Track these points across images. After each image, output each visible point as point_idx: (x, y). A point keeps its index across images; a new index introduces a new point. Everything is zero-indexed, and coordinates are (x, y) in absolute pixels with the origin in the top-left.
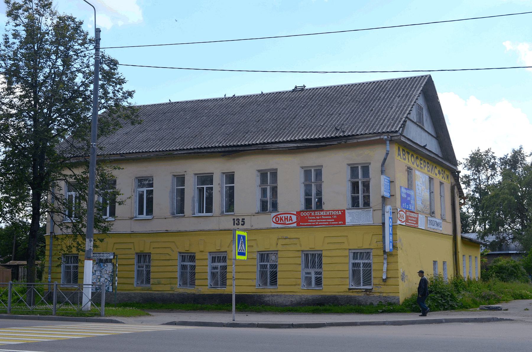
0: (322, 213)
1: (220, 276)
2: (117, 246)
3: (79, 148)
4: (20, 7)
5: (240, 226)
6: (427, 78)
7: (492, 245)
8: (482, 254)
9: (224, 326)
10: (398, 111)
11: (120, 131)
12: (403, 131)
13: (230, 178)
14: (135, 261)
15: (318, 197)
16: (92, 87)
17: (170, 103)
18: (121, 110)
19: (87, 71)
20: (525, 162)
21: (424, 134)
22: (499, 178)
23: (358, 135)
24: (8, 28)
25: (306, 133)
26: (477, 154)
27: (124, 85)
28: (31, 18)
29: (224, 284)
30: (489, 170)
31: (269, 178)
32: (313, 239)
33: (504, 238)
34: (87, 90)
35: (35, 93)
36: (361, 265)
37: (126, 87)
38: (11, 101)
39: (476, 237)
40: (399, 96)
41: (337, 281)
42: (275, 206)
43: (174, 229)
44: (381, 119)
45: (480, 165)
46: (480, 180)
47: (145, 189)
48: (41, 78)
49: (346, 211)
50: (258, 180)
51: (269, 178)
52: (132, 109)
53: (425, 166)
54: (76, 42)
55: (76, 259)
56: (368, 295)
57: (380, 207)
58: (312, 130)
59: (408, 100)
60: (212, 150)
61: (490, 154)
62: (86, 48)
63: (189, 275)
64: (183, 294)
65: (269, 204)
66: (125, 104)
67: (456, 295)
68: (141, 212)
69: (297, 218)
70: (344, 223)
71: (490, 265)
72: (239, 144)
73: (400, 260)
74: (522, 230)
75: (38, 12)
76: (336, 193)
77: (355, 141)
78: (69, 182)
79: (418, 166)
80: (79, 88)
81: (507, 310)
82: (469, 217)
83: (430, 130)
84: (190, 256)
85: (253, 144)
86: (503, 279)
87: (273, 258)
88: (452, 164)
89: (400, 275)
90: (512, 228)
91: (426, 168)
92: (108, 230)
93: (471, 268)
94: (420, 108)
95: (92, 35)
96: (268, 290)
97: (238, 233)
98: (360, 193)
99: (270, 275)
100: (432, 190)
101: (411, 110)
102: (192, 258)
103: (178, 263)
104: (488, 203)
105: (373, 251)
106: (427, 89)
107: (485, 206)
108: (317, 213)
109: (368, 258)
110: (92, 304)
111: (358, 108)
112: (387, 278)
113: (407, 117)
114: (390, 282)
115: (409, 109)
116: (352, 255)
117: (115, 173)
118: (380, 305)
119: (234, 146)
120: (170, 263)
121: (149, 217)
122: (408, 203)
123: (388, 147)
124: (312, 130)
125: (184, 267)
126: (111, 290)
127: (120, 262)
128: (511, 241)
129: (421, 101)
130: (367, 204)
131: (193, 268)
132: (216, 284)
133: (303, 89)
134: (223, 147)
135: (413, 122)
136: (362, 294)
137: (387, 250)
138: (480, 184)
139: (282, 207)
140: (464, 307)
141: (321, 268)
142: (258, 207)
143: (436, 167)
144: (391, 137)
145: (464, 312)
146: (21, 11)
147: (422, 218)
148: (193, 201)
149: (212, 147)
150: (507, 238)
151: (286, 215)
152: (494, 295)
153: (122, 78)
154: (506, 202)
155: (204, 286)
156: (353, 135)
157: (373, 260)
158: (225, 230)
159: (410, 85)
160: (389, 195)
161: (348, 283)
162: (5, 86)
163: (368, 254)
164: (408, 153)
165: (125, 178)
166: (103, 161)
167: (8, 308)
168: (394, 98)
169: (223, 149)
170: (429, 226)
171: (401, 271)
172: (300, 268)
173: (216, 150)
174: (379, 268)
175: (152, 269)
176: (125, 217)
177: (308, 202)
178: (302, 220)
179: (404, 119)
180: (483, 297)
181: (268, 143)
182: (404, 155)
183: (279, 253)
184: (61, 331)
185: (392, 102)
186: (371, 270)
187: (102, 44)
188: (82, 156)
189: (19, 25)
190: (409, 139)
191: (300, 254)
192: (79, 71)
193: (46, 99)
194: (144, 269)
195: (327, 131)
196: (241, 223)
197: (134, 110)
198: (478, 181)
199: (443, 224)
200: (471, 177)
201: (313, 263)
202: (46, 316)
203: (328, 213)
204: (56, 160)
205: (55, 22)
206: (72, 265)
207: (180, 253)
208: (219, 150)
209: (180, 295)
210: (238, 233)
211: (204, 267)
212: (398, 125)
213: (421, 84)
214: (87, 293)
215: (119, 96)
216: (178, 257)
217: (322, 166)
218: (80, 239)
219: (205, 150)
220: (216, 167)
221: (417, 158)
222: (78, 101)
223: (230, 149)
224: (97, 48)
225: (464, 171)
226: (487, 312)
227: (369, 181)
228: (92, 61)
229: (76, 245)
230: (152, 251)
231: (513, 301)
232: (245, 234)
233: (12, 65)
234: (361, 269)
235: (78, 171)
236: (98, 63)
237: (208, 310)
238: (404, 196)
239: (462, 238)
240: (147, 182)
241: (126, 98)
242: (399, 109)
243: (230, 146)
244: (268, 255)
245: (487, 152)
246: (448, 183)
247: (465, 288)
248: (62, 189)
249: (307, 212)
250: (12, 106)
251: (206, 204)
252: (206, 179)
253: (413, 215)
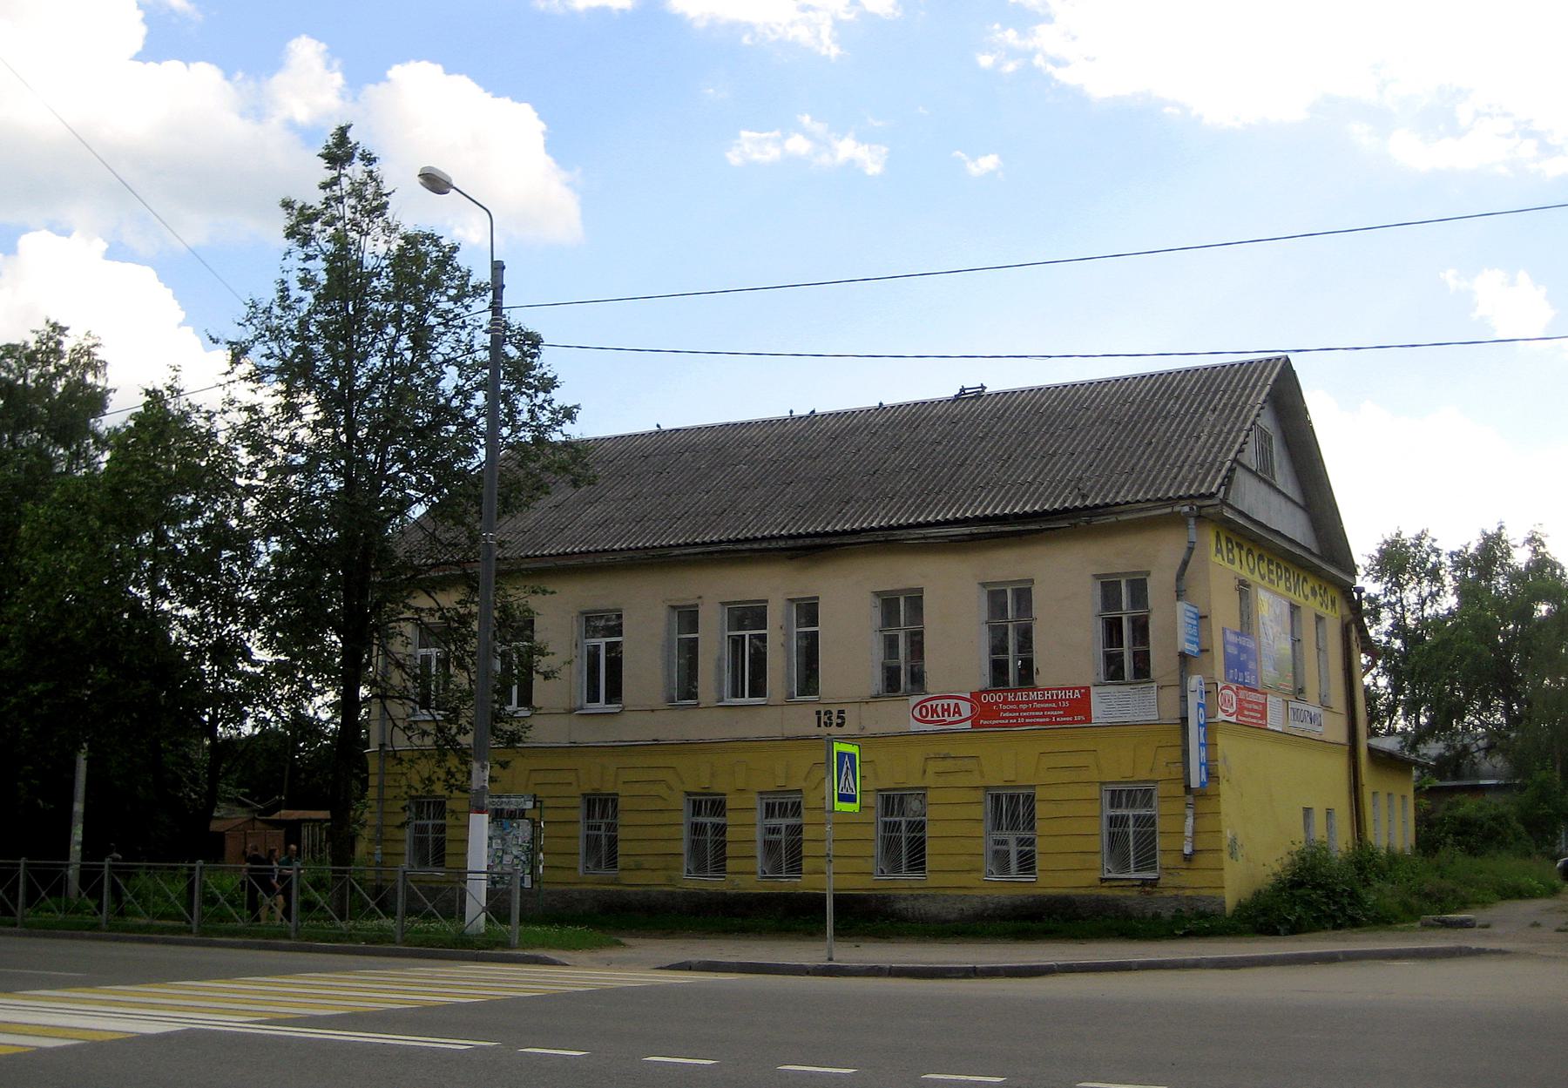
0: (1033, 695)
1: (788, 851)
3: (450, 544)
4: (315, 217)
5: (834, 730)
6: (1280, 364)
7: (1445, 766)
8: (1416, 789)
9: (808, 973)
10: (1213, 445)
11: (545, 502)
12: (1226, 493)
13: (808, 611)
14: (580, 814)
15: (1023, 655)
16: (480, 398)
17: (660, 433)
18: (548, 451)
19: (469, 362)
20: (1511, 561)
21: (1276, 500)
22: (1449, 601)
23: (1117, 504)
24: (287, 264)
25: (992, 500)
26: (1394, 543)
27: (554, 393)
28: (340, 239)
29: (795, 866)
30: (1426, 582)
31: (901, 612)
32: (1010, 761)
33: (1466, 748)
34: (468, 406)
35: (348, 415)
36: (1131, 822)
37: (560, 397)
38: (293, 436)
39: (1398, 747)
40: (1214, 410)
41: (1071, 862)
42: (917, 679)
44: (1173, 466)
45: (1402, 570)
46: (1403, 607)
47: (602, 642)
48: (362, 382)
49: (1093, 690)
50: (877, 618)
51: (901, 612)
52: (577, 450)
53: (1280, 578)
54: (442, 294)
55: (440, 807)
56: (1148, 893)
57: (1175, 678)
58: (1007, 492)
59: (1237, 418)
60: (764, 545)
61: (1426, 543)
62: (467, 307)
63: (710, 848)
65: (902, 675)
66: (556, 437)
67: (1362, 892)
68: (593, 697)
69: (972, 709)
70: (1089, 719)
71: (1439, 815)
72: (828, 529)
73: (1224, 808)
74: (1508, 727)
75: (355, 224)
76: (1067, 646)
77: (1113, 519)
78: (426, 625)
79: (1263, 578)
80: (449, 401)
81: (1487, 926)
82: (1380, 697)
83: (1291, 489)
84: (713, 802)
85: (863, 530)
86: (1472, 851)
87: (915, 805)
88: (1343, 571)
89: (1225, 844)
90: (1483, 724)
91: (1282, 583)
92: (520, 740)
93: (1393, 825)
94: (1265, 437)
95: (482, 275)
96: (903, 883)
97: (839, 747)
98: (1126, 647)
99: (907, 845)
100: (1297, 636)
101: (1245, 443)
102: (718, 807)
103: (685, 818)
104: (1426, 661)
105: (1159, 786)
106: (1280, 390)
107: (1418, 670)
108: (1022, 696)
109: (1148, 803)
110: (488, 920)
111: (1116, 439)
112: (1194, 851)
113: (1235, 460)
114: (1203, 860)
115: (1241, 439)
116: (1108, 796)
117: (534, 602)
118: (1178, 918)
119: (817, 535)
120: (665, 818)
121: (613, 708)
122: (1242, 667)
123: (1192, 533)
124: (1007, 492)
125: (697, 829)
126: (527, 884)
127: (549, 815)
128: (1482, 753)
129: (1267, 421)
130: (1142, 670)
131: (720, 829)
132: (777, 869)
133: (979, 394)
134: (791, 537)
135: (1249, 470)
136: (1133, 893)
137: (1195, 784)
138: (1403, 617)
140: (1382, 920)
141: (1032, 828)
142: (876, 681)
143: (1305, 580)
144: (1200, 508)
145: (1383, 933)
146: (317, 226)
147: (1275, 706)
148: (720, 668)
149: (764, 538)
150: (1474, 748)
151: (945, 702)
152: (1454, 891)
153: (550, 375)
154: (1468, 660)
155: (749, 875)
156: (1107, 505)
157: (1158, 809)
158: (797, 738)
159: (1240, 381)
160: (1195, 649)
161: (1099, 865)
162: (280, 399)
163: (1148, 794)
164: (1240, 547)
165: (556, 616)
166: (511, 572)
167: (292, 925)
168: (1203, 414)
169: (791, 543)
170: (1291, 723)
171: (1228, 834)
172: (980, 830)
173: (774, 544)
174: (1177, 829)
175: (622, 833)
176: (555, 707)
177: (999, 669)
178: (984, 713)
179: (1228, 464)
180: (1428, 896)
181: (900, 527)
182: (1230, 551)
183: (929, 793)
184: (425, 985)
185: (1197, 423)
186: (1154, 832)
187: (508, 299)
188: (458, 563)
189: (315, 257)
190: (1241, 513)
191: (979, 795)
192: (448, 361)
193: (374, 429)
194: (602, 832)
195: (1041, 495)
196: (835, 720)
197: (577, 451)
198: (1398, 609)
199: (1326, 717)
200: (1383, 600)
201: (1014, 817)
202: (379, 946)
203: (1048, 695)
204: (396, 572)
205: (394, 247)
206: (430, 822)
207: (688, 794)
208: (782, 544)
209: (689, 896)
210: (839, 747)
211: (747, 828)
212: (1214, 479)
213: (1267, 378)
214: (477, 893)
215: (544, 419)
216: (683, 804)
217: (1032, 581)
218: (453, 762)
219: (747, 546)
220: (773, 587)
221: (1261, 557)
222: (447, 431)
223: (808, 541)
224: (496, 308)
225: (1370, 586)
226: (1443, 932)
227: (1147, 617)
228: (483, 339)
229: (443, 776)
230: (621, 790)
231: (1500, 903)
232: (854, 749)
233: (296, 351)
234: (1131, 830)
235: (449, 599)
236: (495, 347)
237: (760, 933)
238: (1232, 650)
239: (1371, 750)
240: (603, 623)
241: (559, 423)
242: (1216, 440)
243: (808, 535)
244: (902, 797)
245: (1419, 538)
246: (1334, 617)
247: (1382, 874)
248: (406, 642)
249: (995, 692)
250: (295, 447)
251: (751, 674)
252: (750, 615)
253: (1253, 696)
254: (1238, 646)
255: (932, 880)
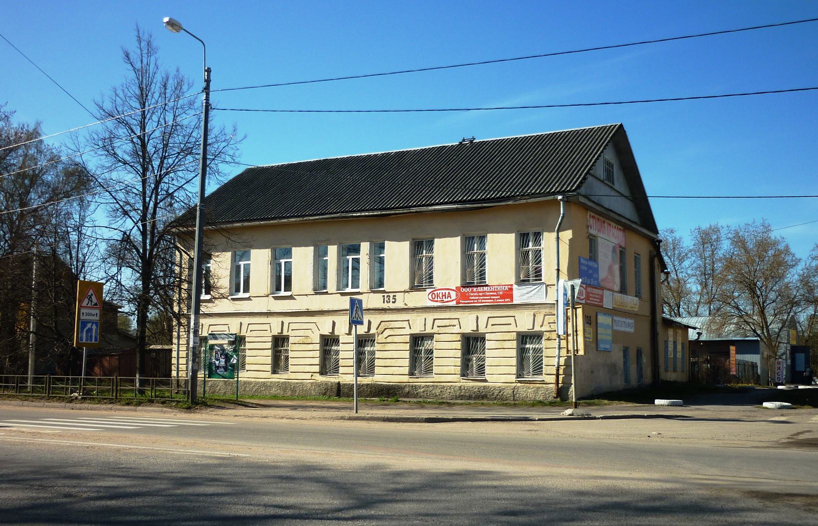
0: (485, 289)
2: (492, 321)
43: (314, 308)
64: (87, 397)
96: (422, 381)
106: (618, 138)
135: (599, 180)
139: (437, 283)
230: (290, 333)
234: (30, 375)
254: (587, 266)
255: (437, 378)
